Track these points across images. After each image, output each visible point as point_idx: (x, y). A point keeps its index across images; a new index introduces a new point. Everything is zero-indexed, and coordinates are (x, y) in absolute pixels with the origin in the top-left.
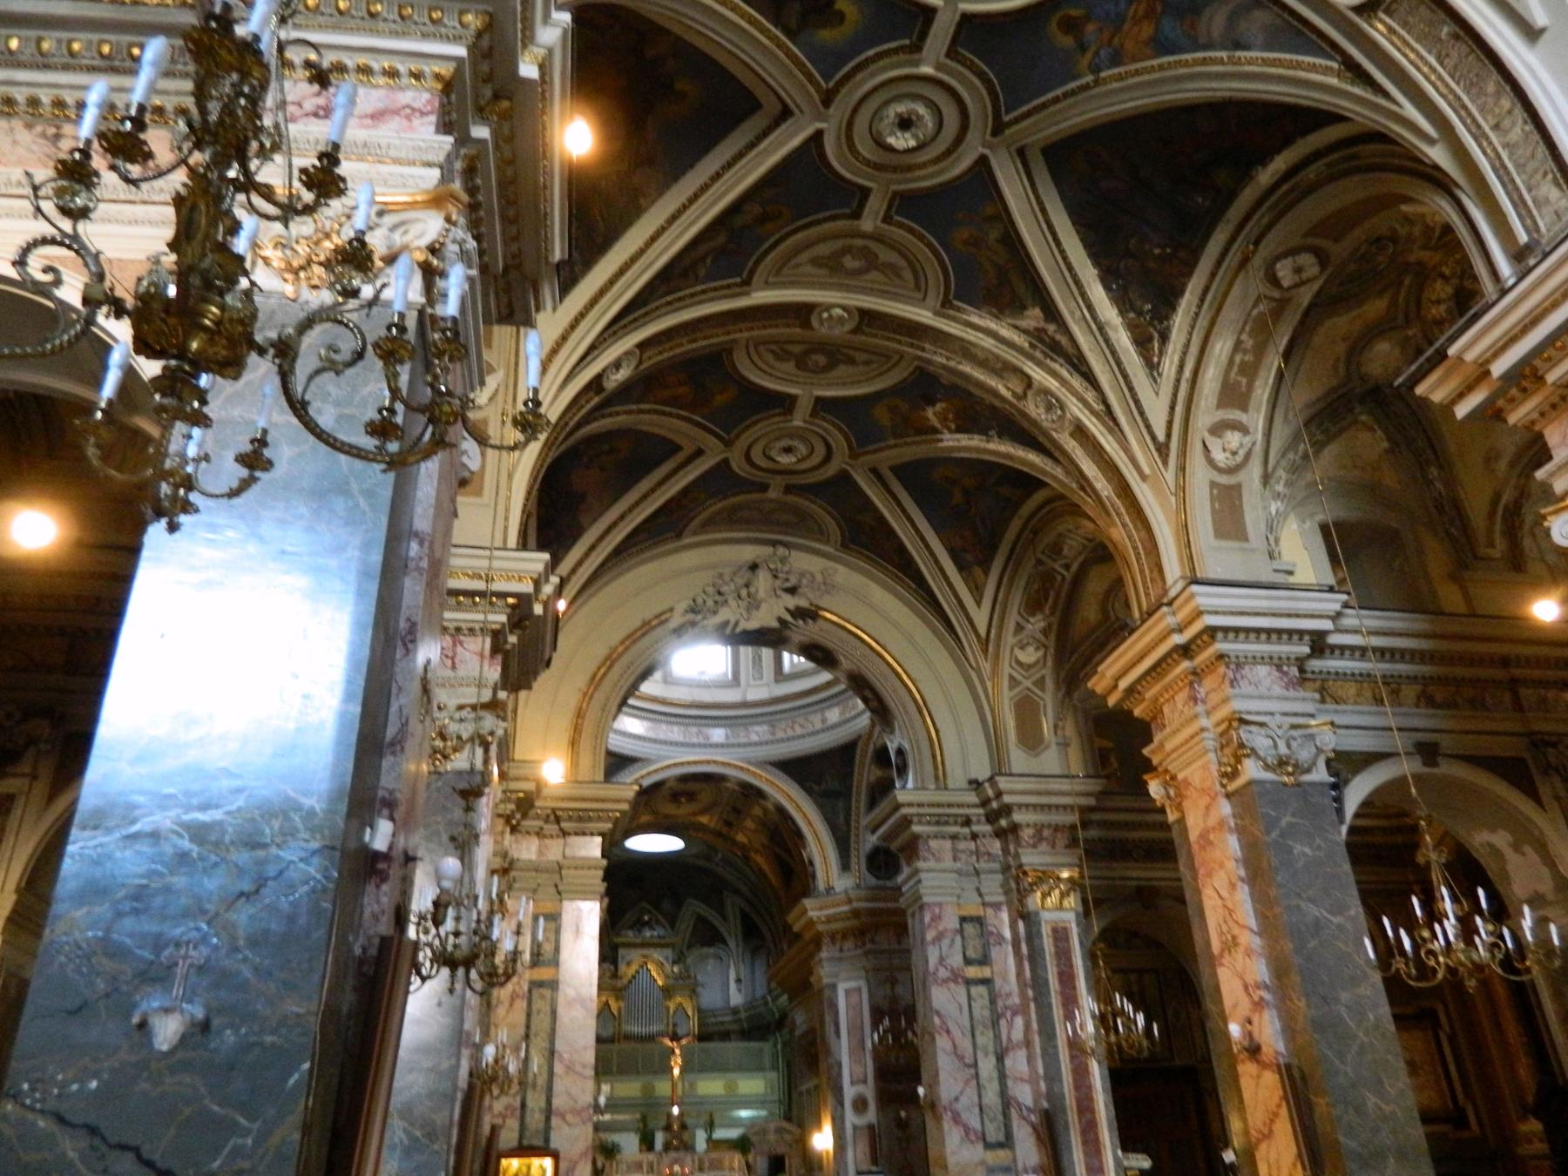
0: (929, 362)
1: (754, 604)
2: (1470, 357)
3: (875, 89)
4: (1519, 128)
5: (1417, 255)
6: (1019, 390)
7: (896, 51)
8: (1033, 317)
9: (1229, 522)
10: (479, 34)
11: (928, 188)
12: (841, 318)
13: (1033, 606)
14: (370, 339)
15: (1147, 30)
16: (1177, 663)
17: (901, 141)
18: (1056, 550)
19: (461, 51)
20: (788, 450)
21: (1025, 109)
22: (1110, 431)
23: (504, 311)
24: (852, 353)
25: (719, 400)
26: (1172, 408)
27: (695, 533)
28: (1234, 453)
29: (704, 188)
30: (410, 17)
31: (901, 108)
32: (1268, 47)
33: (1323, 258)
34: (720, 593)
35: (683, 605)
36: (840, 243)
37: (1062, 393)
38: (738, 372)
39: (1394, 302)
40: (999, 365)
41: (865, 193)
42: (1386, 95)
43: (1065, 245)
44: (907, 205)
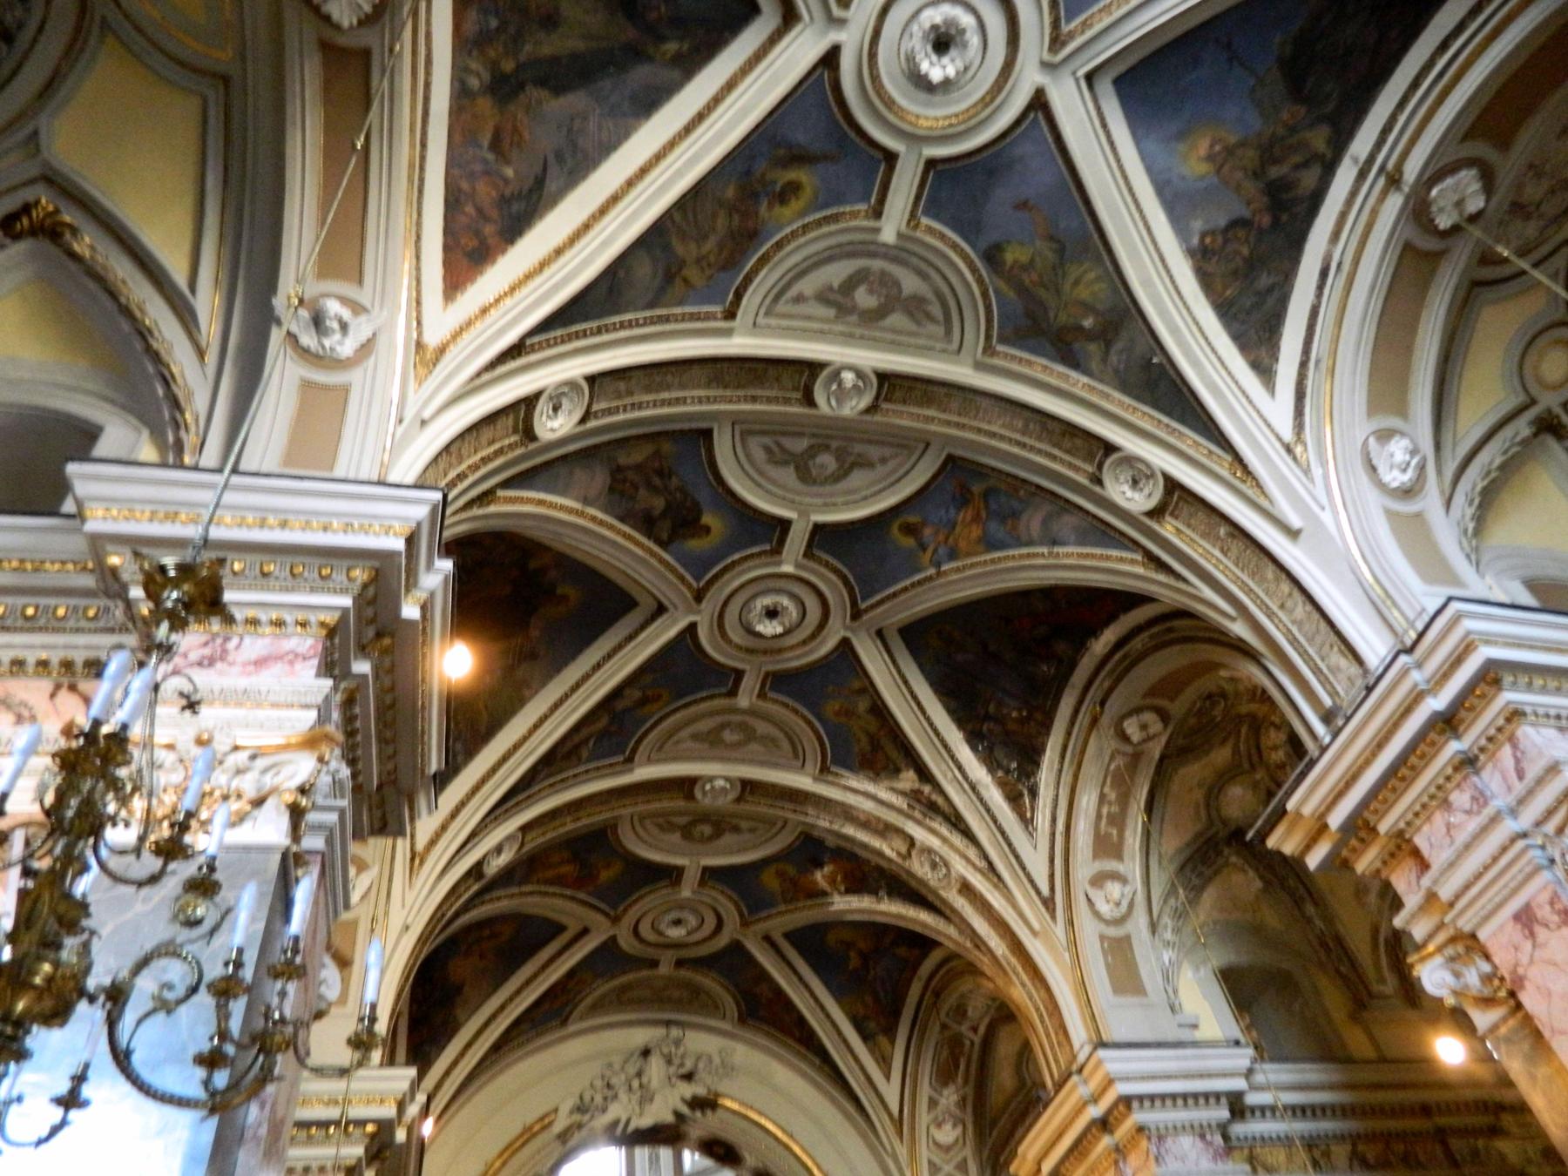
0: (813, 826)
1: (646, 1098)
2: (1307, 810)
3: (742, 586)
4: (1301, 609)
5: (1245, 708)
6: (904, 850)
7: (759, 554)
8: (908, 779)
9: (1126, 979)
10: (365, 586)
11: (797, 669)
12: (723, 789)
13: (944, 1076)
14: (207, 978)
15: (976, 532)
16: (1098, 1140)
17: (770, 628)
18: (960, 1012)
19: (346, 601)
20: (677, 922)
21: (878, 597)
22: (996, 886)
23: (377, 825)
24: (735, 821)
25: (605, 875)
26: (1052, 861)
27: (581, 1018)
28: (1118, 904)
29: (586, 677)
30: (301, 574)
31: (767, 601)
32: (1081, 542)
33: (1164, 717)
34: (609, 1086)
35: (565, 1108)
36: (719, 719)
37: (945, 851)
38: (624, 848)
39: (1236, 751)
40: (881, 826)
41: (739, 675)
42: (1185, 580)
43: (929, 711)
44: (779, 682)
